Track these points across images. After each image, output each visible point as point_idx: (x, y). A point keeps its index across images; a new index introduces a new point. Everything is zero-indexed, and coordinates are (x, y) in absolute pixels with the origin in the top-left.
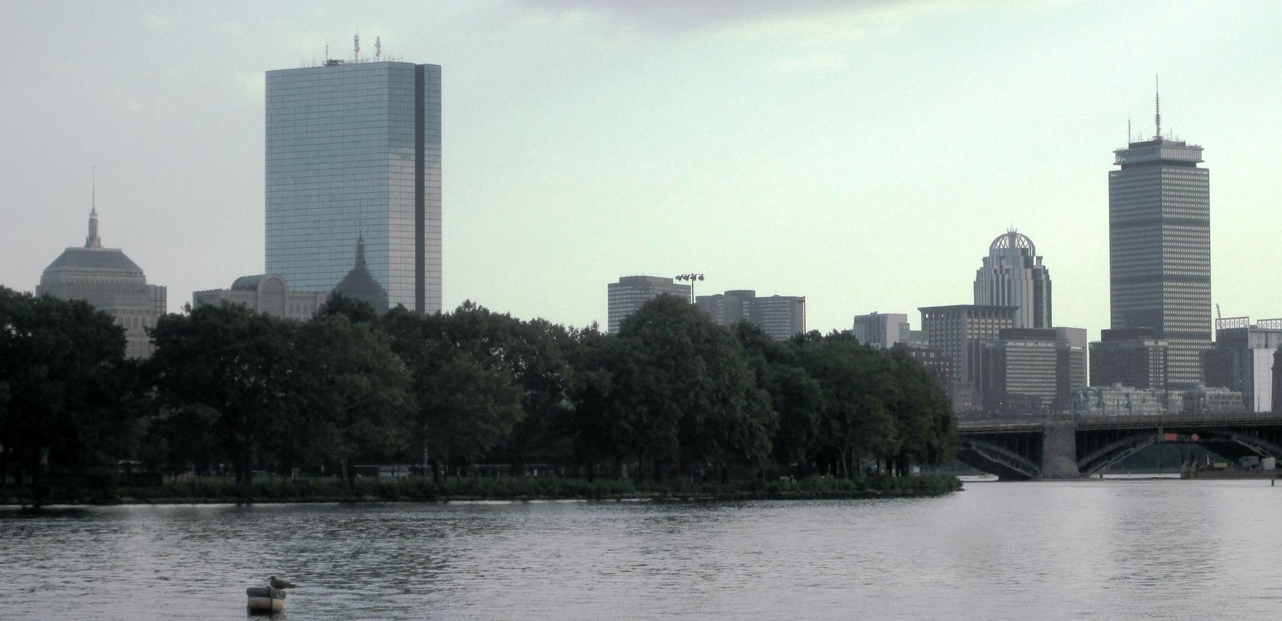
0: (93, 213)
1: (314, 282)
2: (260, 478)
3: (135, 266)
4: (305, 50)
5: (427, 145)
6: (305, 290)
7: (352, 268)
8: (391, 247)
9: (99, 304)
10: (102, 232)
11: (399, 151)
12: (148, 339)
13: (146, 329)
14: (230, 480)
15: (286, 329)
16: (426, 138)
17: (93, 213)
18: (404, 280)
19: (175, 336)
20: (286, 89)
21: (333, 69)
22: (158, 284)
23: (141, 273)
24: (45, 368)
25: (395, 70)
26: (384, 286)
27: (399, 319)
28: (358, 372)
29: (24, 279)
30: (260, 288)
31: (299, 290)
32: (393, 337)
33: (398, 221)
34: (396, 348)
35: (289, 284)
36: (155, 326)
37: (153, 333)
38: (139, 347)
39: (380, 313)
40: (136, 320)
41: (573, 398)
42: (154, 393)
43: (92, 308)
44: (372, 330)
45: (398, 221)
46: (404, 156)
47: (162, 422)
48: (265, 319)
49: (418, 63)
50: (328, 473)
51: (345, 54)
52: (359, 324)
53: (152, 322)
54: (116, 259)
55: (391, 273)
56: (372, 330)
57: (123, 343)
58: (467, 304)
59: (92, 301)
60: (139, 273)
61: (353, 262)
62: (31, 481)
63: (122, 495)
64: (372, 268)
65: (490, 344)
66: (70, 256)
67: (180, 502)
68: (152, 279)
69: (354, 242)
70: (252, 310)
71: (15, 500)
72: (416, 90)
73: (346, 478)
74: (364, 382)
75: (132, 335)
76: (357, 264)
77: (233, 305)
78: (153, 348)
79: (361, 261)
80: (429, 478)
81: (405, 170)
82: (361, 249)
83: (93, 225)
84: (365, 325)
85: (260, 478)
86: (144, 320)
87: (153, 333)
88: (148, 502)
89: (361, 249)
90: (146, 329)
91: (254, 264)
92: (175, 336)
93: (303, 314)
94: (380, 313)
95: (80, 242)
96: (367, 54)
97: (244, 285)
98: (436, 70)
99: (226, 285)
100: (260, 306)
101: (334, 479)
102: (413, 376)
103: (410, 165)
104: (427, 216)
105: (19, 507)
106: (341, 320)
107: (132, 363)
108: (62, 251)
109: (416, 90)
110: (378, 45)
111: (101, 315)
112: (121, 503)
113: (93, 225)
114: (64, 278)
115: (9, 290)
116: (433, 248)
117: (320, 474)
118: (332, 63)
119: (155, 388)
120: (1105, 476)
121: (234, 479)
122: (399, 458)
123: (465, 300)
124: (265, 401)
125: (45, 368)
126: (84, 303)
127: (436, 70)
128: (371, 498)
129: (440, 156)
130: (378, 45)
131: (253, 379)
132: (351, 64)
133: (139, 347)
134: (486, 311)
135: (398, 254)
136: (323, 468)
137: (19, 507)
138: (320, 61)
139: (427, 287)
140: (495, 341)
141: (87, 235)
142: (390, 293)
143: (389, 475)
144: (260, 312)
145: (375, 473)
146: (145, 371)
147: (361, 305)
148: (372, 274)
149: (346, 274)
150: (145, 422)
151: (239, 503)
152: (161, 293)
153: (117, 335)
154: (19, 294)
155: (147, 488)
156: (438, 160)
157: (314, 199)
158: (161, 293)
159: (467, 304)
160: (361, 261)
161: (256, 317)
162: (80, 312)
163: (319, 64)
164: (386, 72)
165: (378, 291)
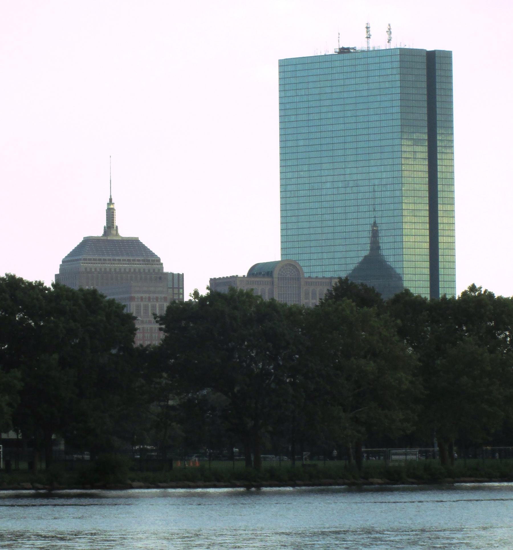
0: (111, 202)
1: (335, 262)
2: (270, 461)
3: (153, 254)
4: (319, 42)
5: (439, 131)
6: (320, 275)
7: (367, 253)
8: (405, 232)
9: (110, 292)
10: (118, 222)
11: (415, 136)
12: (157, 326)
13: (154, 315)
14: (240, 465)
15: (293, 314)
16: (439, 124)
17: (111, 202)
18: (418, 264)
19: (183, 323)
20: (299, 79)
21: (346, 56)
22: (175, 272)
23: (159, 260)
24: (56, 356)
25: (407, 56)
26: (398, 271)
27: (406, 302)
28: (365, 357)
29: (42, 269)
30: (276, 275)
31: (314, 275)
32: (399, 321)
33: (411, 207)
34: (402, 332)
35: (305, 269)
36: (164, 312)
37: (162, 320)
38: (149, 334)
39: (387, 296)
40: (146, 307)
41: (54, 440)
42: (164, 379)
43: (102, 296)
44: (378, 315)
45: (411, 207)
46: (416, 142)
47: (173, 408)
48: (272, 305)
49: (429, 48)
50: (339, 457)
51: (359, 43)
52: (365, 309)
53: (161, 308)
54: (134, 246)
55: (405, 257)
56: (378, 315)
57: (133, 330)
58: (473, 288)
59: (101, 290)
60: (157, 260)
61: (368, 247)
62: (44, 466)
63: (133, 480)
64: (387, 253)
65: (496, 328)
66: (88, 244)
67: (189, 487)
68: (169, 267)
69: (369, 228)
70: (260, 297)
71: (29, 485)
72: (427, 77)
73: (353, 461)
74: (371, 366)
75: (142, 322)
76: (372, 249)
77: (241, 291)
78: (162, 335)
79: (375, 246)
80: (436, 462)
81: (419, 155)
82: (375, 234)
83: (110, 214)
84: (372, 310)
85: (270, 461)
86: (154, 307)
87: (162, 320)
88: (158, 487)
89: (375, 234)
90: (154, 315)
91: (269, 250)
92: (183, 323)
93: (310, 300)
94: (387, 296)
95: (99, 232)
96: (379, 43)
97: (259, 271)
98: (447, 56)
99: (243, 271)
100: (264, 292)
101: (342, 463)
102: (420, 360)
103: (423, 151)
104: (440, 201)
105: (32, 492)
106: (348, 304)
107: (142, 351)
108: (81, 240)
109: (427, 77)
110: (389, 32)
111: (112, 302)
112: (132, 487)
113: (110, 214)
114: (83, 266)
115: (21, 280)
116: (447, 233)
117: (332, 458)
118: (344, 51)
119: (165, 375)
120: (264, 489)
121: (243, 463)
122: (408, 441)
123: (470, 284)
124: (273, 386)
125: (56, 356)
126: (94, 292)
127: (447, 56)
128: (379, 481)
129: (452, 141)
130: (389, 32)
131: (260, 365)
132: (363, 51)
133: (149, 334)
134: (491, 296)
135: (412, 239)
136: (335, 453)
137: (32, 492)
138: (331, 49)
139: (441, 271)
140: (501, 326)
141: (105, 224)
142: (405, 277)
143: (400, 457)
144: (267, 298)
145: (387, 457)
146: (152, 358)
147: (368, 290)
148: (387, 259)
149: (360, 259)
150: (155, 408)
151: (248, 487)
152: (178, 280)
153: (127, 322)
154: (30, 284)
155: (161, 472)
156: (450, 145)
157: (328, 185)
158: (178, 280)
159: (473, 288)
160: (375, 246)
161: (263, 304)
162: (91, 300)
163: (331, 52)
164: (398, 58)
165: (392, 275)
